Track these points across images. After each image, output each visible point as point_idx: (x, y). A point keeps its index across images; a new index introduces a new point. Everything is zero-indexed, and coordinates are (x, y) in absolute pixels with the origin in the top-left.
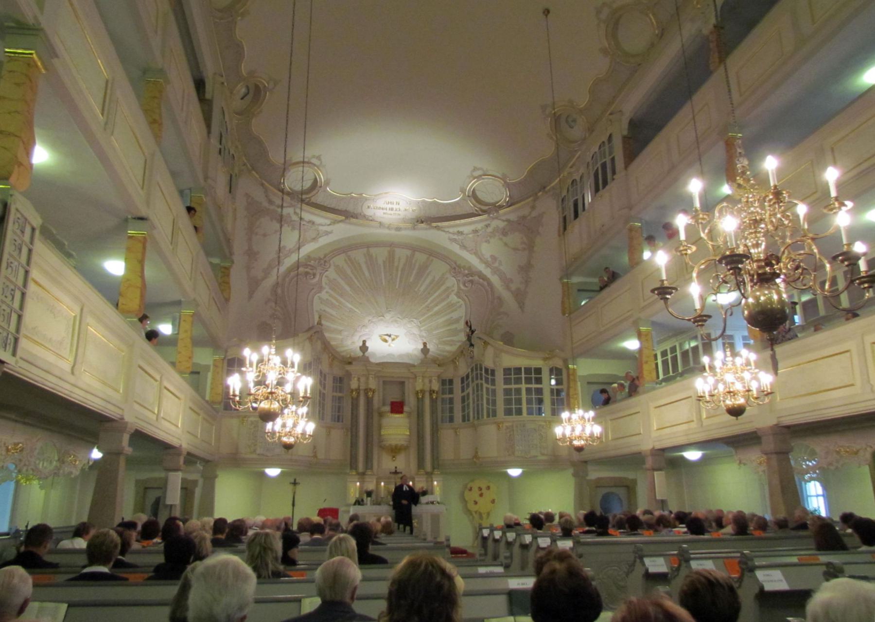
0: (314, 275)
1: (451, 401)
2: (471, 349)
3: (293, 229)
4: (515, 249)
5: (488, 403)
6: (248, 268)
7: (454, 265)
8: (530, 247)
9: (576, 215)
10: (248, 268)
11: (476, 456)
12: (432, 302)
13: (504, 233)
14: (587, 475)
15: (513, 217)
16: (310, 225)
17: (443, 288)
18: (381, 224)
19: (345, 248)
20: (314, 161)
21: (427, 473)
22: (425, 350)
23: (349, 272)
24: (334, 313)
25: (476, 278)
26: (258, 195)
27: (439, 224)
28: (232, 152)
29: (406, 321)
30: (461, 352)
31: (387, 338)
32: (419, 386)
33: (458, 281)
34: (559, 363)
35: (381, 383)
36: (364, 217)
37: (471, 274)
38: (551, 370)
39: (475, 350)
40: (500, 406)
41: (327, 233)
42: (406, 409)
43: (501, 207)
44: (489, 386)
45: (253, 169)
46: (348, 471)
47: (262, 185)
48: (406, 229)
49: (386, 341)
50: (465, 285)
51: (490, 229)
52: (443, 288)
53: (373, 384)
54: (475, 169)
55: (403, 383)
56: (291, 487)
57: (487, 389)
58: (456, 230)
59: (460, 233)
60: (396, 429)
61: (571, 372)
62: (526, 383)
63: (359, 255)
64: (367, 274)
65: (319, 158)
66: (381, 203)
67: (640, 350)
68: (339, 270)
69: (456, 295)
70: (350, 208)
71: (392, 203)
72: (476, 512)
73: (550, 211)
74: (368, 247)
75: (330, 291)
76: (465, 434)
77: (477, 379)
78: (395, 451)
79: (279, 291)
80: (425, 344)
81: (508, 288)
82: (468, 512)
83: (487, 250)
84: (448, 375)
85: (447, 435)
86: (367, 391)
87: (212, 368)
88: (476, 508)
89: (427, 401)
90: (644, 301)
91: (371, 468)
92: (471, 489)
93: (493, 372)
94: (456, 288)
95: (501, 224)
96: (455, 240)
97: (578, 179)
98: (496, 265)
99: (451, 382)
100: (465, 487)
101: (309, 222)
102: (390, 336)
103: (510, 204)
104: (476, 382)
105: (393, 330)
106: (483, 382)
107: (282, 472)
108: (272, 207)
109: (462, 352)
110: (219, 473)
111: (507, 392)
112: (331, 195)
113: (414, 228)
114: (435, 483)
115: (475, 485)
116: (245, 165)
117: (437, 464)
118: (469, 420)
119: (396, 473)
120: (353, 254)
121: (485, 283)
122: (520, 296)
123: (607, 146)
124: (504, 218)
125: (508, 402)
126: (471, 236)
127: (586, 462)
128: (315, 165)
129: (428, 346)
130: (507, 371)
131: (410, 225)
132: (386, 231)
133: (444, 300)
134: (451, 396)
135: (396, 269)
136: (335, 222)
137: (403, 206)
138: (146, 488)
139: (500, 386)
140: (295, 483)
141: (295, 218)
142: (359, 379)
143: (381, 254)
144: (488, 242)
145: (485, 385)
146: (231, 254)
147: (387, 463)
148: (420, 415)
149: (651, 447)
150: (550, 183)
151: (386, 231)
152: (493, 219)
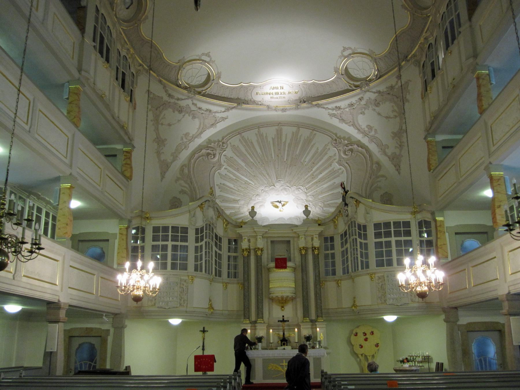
0: (214, 155)
1: (333, 256)
2: (346, 208)
3: (194, 117)
4: (387, 117)
5: (362, 257)
6: (158, 153)
7: (335, 137)
8: (402, 113)
9: (434, 76)
10: (158, 153)
11: (354, 305)
12: (321, 166)
13: (377, 104)
14: (458, 320)
15: (382, 88)
16: (208, 113)
17: (326, 157)
18: (268, 107)
19: (239, 130)
20: (204, 58)
21: (312, 321)
22: (307, 212)
23: (243, 149)
24: (232, 186)
25: (355, 146)
26: (157, 89)
27: (320, 102)
28: (123, 53)
29: (294, 188)
30: (339, 212)
31: (278, 204)
32: (302, 243)
33: (339, 151)
34: (427, 217)
35: (269, 243)
36: (254, 102)
37: (351, 144)
38: (420, 224)
39: (349, 209)
40: (373, 259)
41: (224, 119)
42: (289, 264)
43: (370, 81)
44: (363, 241)
45: (151, 69)
46: (242, 320)
47: (160, 81)
48: (290, 109)
49: (277, 207)
50: (345, 153)
51: (363, 102)
52: (326, 157)
53: (261, 243)
54: (345, 49)
55: (288, 242)
56: (201, 333)
57: (361, 243)
58: (334, 106)
59: (339, 108)
60: (282, 282)
61: (438, 224)
62: (395, 236)
63: (252, 135)
64: (259, 151)
65: (208, 55)
66: (267, 89)
67: (493, 199)
68: (235, 149)
69: (337, 162)
70: (242, 96)
71: (277, 88)
72: (362, 355)
73: (413, 75)
74: (259, 127)
75: (228, 167)
76: (345, 284)
77: (352, 235)
78: (283, 302)
79: (186, 171)
80: (306, 207)
81: (385, 154)
82: (355, 354)
83: (363, 121)
84: (329, 233)
85: (330, 286)
86: (256, 250)
87: (118, 235)
88: (361, 351)
89: (310, 257)
90: (494, 145)
91: (262, 318)
92: (356, 335)
93: (365, 227)
94: (337, 157)
95: (373, 96)
96: (334, 115)
97: (433, 42)
98: (373, 133)
99: (332, 239)
100: (351, 332)
101: (207, 110)
102: (280, 202)
103: (378, 77)
104: (352, 238)
105: (283, 197)
106: (357, 237)
107: (182, 322)
108: (172, 101)
109: (340, 212)
110: (127, 322)
111: (379, 245)
112: (223, 86)
113: (297, 108)
114: (318, 329)
115: (360, 332)
116: (141, 65)
117: (321, 312)
118: (348, 273)
119: (283, 321)
120: (245, 135)
121: (364, 151)
122: (395, 159)
123: (453, 5)
124: (374, 90)
125: (379, 254)
126: (347, 110)
127: (456, 308)
128: (205, 61)
129: (309, 209)
130: (377, 226)
131: (294, 106)
132: (274, 113)
133: (326, 168)
134: (333, 251)
135: (282, 144)
136: (228, 109)
137: (286, 89)
138: (71, 337)
139: (372, 240)
140: (204, 331)
141: (193, 108)
142: (249, 241)
143: (271, 132)
144: (363, 113)
145: (359, 240)
146: (131, 140)
147: (277, 313)
148: (304, 269)
149: (506, 292)
150: (412, 52)
151: (274, 113)
152: (365, 92)
